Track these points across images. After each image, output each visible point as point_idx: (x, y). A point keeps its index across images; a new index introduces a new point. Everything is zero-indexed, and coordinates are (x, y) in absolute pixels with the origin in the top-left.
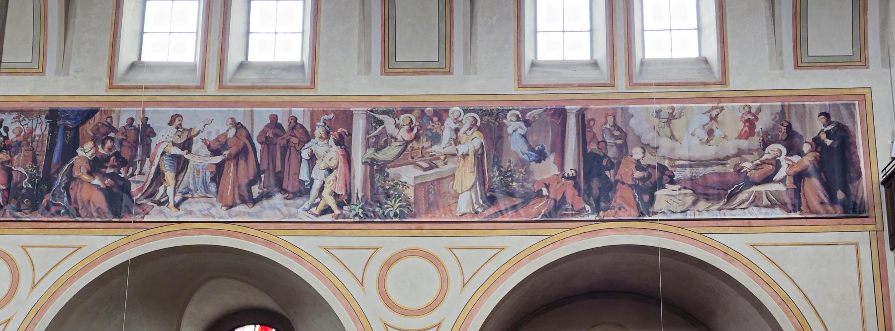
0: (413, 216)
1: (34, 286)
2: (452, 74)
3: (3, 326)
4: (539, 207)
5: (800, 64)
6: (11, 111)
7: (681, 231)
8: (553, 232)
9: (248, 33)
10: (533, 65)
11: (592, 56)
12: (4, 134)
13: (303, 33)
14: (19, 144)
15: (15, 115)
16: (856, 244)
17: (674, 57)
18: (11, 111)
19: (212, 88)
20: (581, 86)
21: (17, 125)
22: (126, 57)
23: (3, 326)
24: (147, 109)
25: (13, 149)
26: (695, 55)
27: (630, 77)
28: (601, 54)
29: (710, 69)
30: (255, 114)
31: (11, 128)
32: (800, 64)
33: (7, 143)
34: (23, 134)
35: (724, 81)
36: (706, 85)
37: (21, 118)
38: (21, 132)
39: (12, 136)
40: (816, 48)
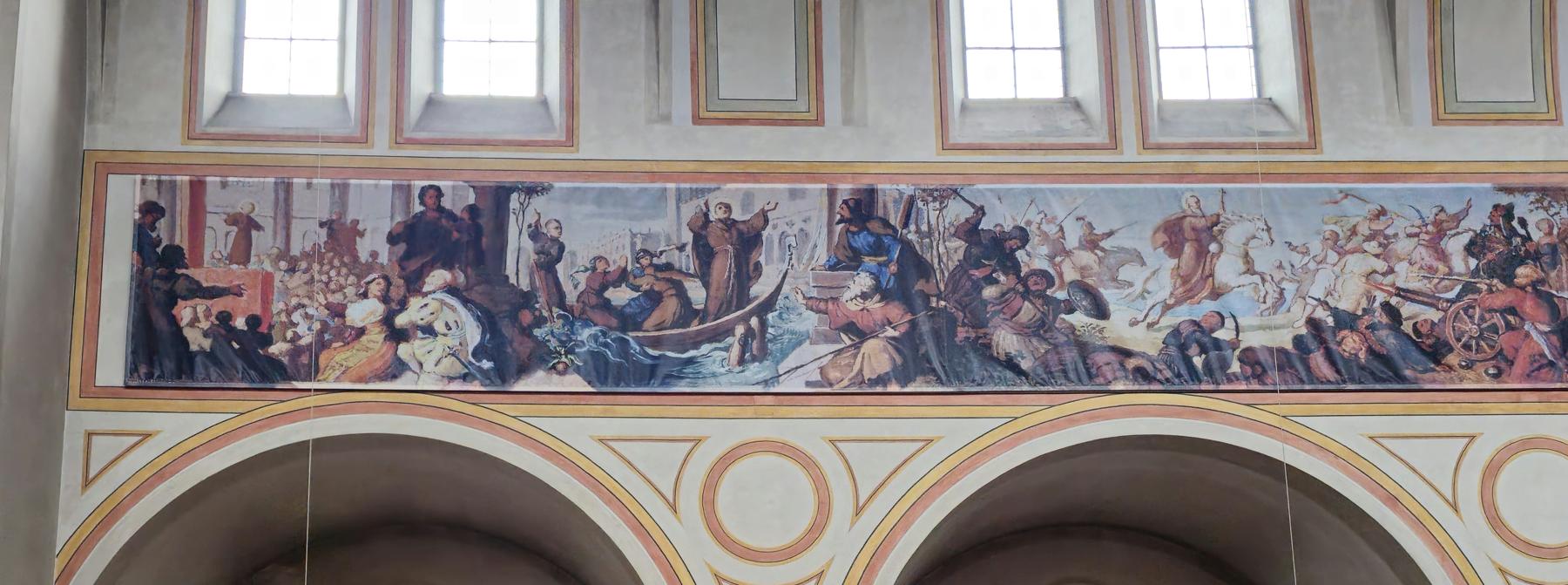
0: (308, 378)
1: (858, 511)
2: (1561, 124)
3: (1511, 580)
4: (1132, 363)
5: (1443, 116)
6: (1525, 190)
7: (1285, 424)
8: (1014, 411)
9: (1064, 48)
10: (964, 107)
11: (1066, 93)
12: (1523, 232)
13: (1157, 49)
14: (1554, 249)
15: (1533, 196)
16: (90, 435)
17: (1216, 96)
18: (1525, 190)
19: (1130, 151)
20: (1022, 149)
21: (1542, 214)
22: (215, 84)
23: (1511, 580)
24: (315, 181)
25: (1546, 259)
26: (1249, 93)
27: (398, 128)
28: (1088, 87)
29: (1087, 119)
30: (352, 192)
31: (1532, 220)
32: (1552, 115)
33: (1530, 247)
34: (1555, 231)
35: (1313, 145)
36: (1225, 144)
37: (1546, 203)
38: (1551, 227)
39: (1536, 235)
40: (734, 84)
